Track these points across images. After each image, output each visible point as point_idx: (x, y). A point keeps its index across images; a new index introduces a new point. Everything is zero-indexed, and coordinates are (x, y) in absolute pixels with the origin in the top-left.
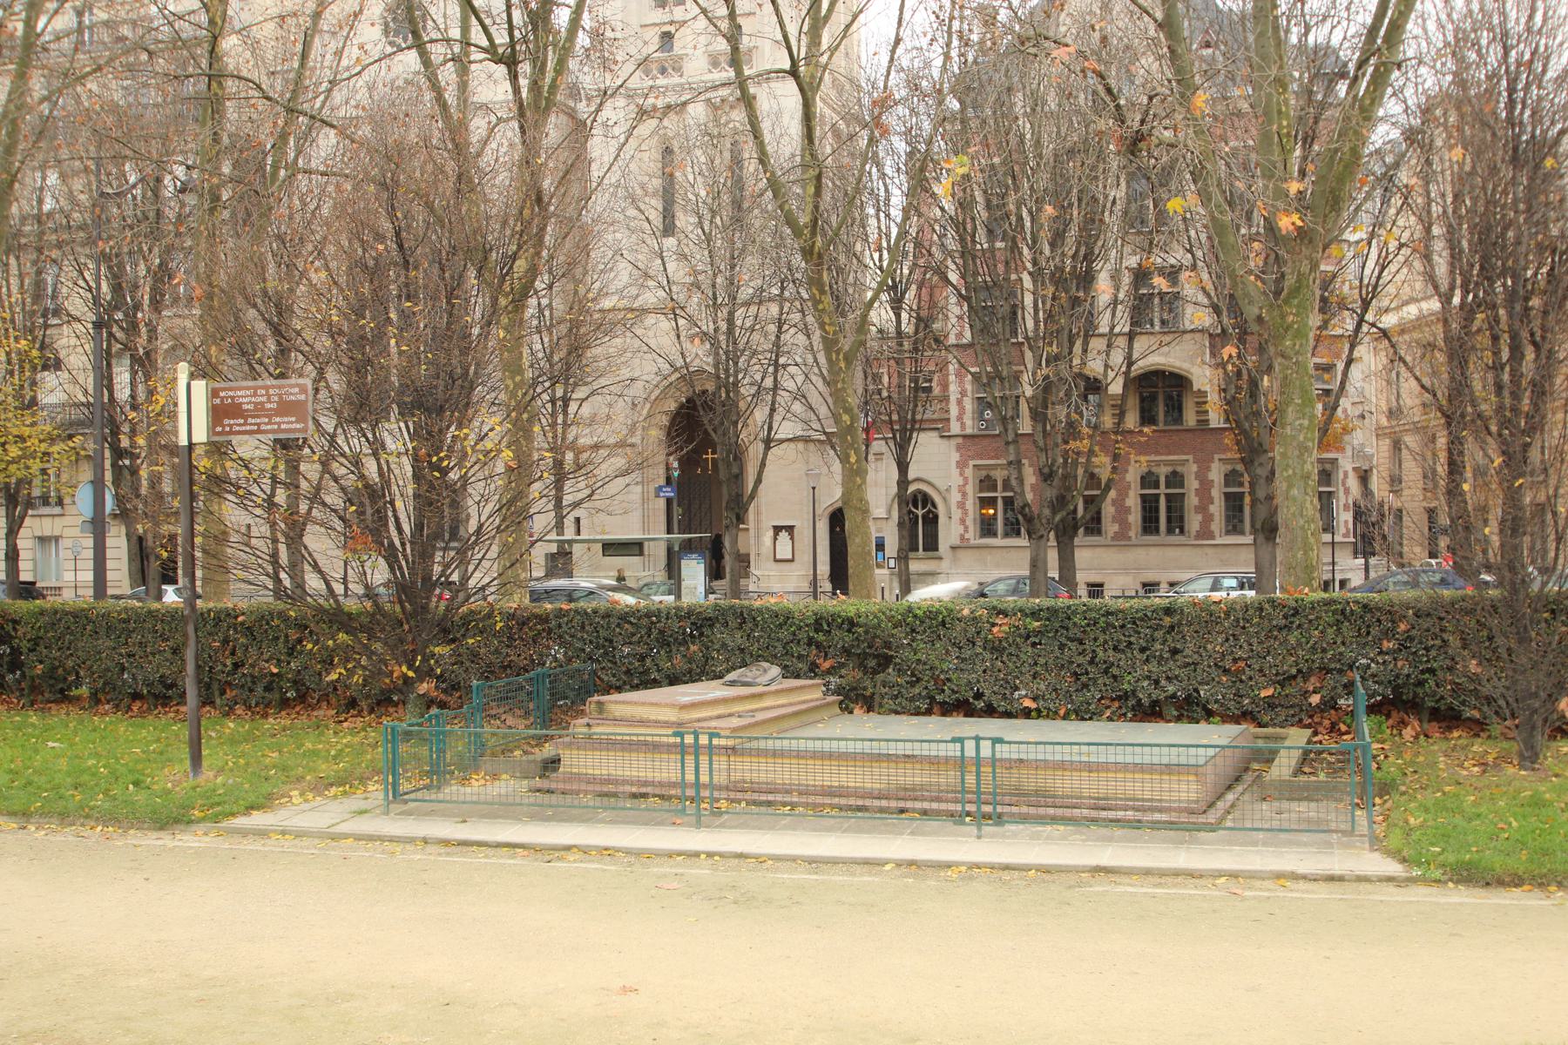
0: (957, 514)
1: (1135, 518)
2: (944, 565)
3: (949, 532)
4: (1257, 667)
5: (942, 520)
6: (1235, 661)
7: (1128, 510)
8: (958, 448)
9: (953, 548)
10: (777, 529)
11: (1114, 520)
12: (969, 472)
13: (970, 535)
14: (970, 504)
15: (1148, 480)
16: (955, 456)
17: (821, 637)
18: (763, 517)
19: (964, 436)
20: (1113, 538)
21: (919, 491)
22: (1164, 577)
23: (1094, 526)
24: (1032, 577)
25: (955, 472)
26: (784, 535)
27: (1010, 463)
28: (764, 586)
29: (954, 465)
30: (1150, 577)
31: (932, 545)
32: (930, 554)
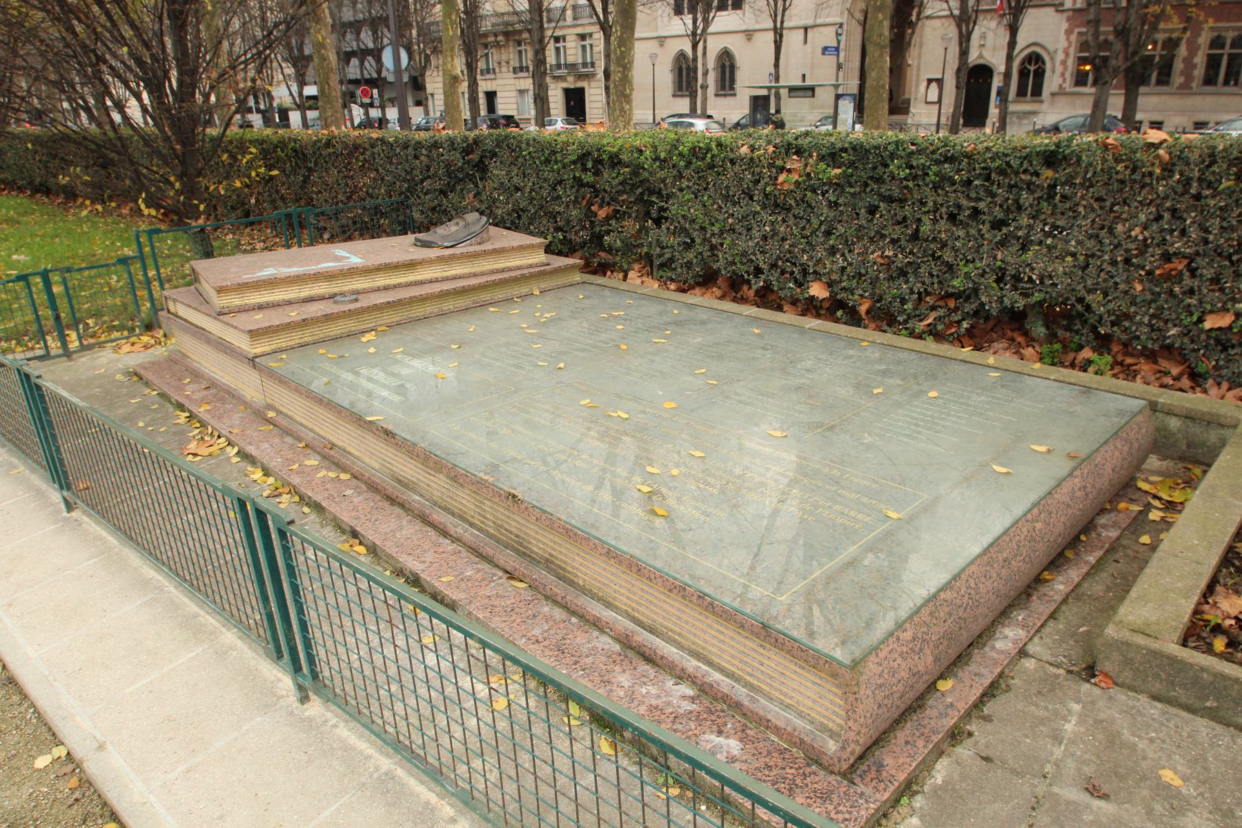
0: (1059, 69)
1: (1199, 72)
2: (1044, 107)
3: (1052, 82)
4: (1208, 273)
5: (1048, 74)
6: (1167, 257)
7: (1194, 66)
8: (1068, 19)
9: (1053, 94)
10: (930, 81)
11: (1182, 73)
12: (1073, 37)
13: (1066, 85)
14: (1070, 62)
15: (1217, 43)
16: (1065, 26)
17: (588, 178)
18: (922, 72)
19: (1075, 10)
20: (1178, 88)
21: (1034, 53)
22: (1212, 118)
23: (1164, 78)
24: (1093, 115)
25: (1063, 37)
26: (934, 85)
27: (1089, 22)
28: (917, 120)
29: (1063, 32)
30: (1202, 117)
31: (1037, 92)
32: (1035, 98)
